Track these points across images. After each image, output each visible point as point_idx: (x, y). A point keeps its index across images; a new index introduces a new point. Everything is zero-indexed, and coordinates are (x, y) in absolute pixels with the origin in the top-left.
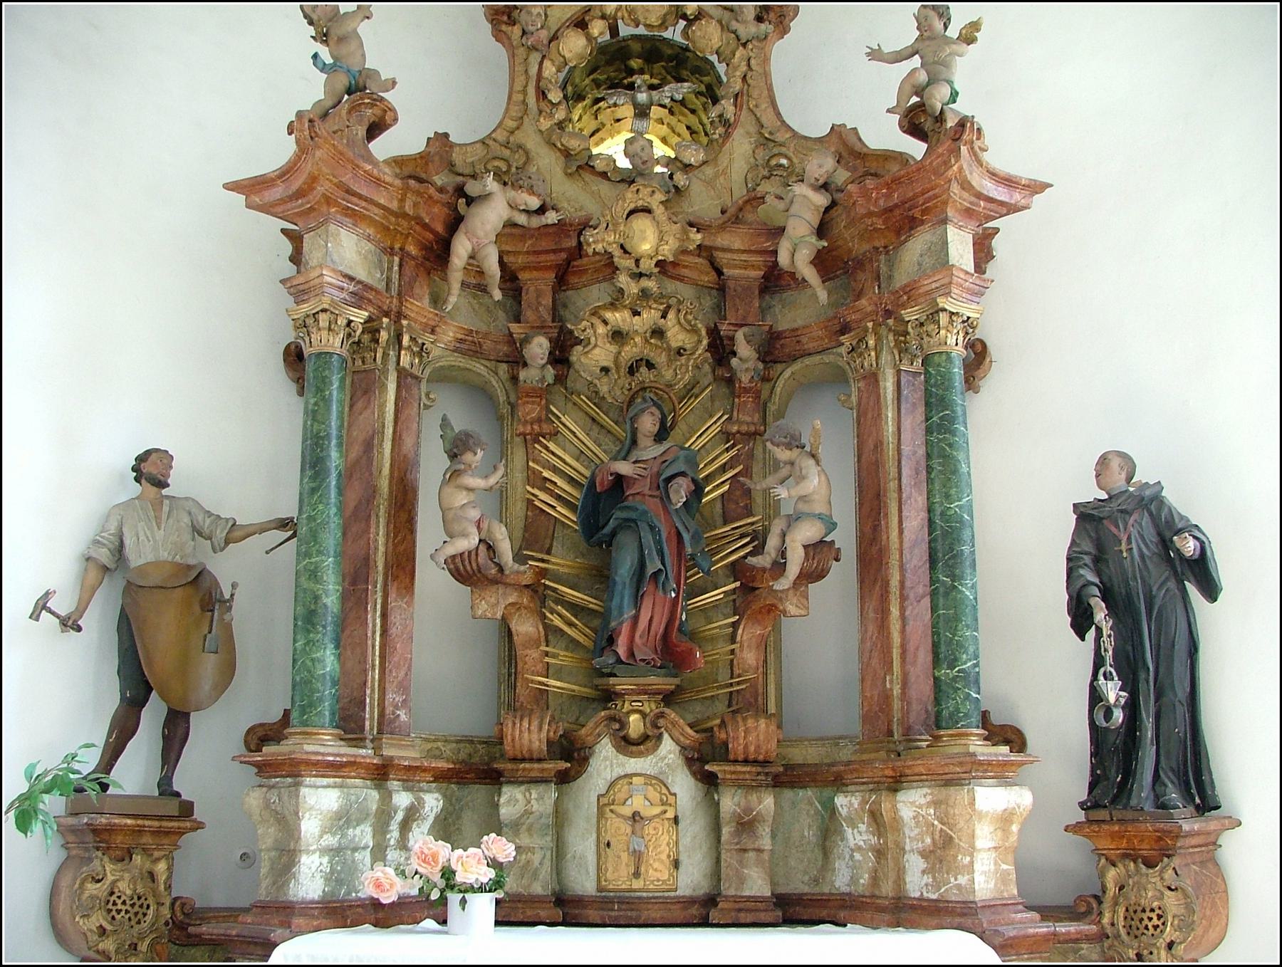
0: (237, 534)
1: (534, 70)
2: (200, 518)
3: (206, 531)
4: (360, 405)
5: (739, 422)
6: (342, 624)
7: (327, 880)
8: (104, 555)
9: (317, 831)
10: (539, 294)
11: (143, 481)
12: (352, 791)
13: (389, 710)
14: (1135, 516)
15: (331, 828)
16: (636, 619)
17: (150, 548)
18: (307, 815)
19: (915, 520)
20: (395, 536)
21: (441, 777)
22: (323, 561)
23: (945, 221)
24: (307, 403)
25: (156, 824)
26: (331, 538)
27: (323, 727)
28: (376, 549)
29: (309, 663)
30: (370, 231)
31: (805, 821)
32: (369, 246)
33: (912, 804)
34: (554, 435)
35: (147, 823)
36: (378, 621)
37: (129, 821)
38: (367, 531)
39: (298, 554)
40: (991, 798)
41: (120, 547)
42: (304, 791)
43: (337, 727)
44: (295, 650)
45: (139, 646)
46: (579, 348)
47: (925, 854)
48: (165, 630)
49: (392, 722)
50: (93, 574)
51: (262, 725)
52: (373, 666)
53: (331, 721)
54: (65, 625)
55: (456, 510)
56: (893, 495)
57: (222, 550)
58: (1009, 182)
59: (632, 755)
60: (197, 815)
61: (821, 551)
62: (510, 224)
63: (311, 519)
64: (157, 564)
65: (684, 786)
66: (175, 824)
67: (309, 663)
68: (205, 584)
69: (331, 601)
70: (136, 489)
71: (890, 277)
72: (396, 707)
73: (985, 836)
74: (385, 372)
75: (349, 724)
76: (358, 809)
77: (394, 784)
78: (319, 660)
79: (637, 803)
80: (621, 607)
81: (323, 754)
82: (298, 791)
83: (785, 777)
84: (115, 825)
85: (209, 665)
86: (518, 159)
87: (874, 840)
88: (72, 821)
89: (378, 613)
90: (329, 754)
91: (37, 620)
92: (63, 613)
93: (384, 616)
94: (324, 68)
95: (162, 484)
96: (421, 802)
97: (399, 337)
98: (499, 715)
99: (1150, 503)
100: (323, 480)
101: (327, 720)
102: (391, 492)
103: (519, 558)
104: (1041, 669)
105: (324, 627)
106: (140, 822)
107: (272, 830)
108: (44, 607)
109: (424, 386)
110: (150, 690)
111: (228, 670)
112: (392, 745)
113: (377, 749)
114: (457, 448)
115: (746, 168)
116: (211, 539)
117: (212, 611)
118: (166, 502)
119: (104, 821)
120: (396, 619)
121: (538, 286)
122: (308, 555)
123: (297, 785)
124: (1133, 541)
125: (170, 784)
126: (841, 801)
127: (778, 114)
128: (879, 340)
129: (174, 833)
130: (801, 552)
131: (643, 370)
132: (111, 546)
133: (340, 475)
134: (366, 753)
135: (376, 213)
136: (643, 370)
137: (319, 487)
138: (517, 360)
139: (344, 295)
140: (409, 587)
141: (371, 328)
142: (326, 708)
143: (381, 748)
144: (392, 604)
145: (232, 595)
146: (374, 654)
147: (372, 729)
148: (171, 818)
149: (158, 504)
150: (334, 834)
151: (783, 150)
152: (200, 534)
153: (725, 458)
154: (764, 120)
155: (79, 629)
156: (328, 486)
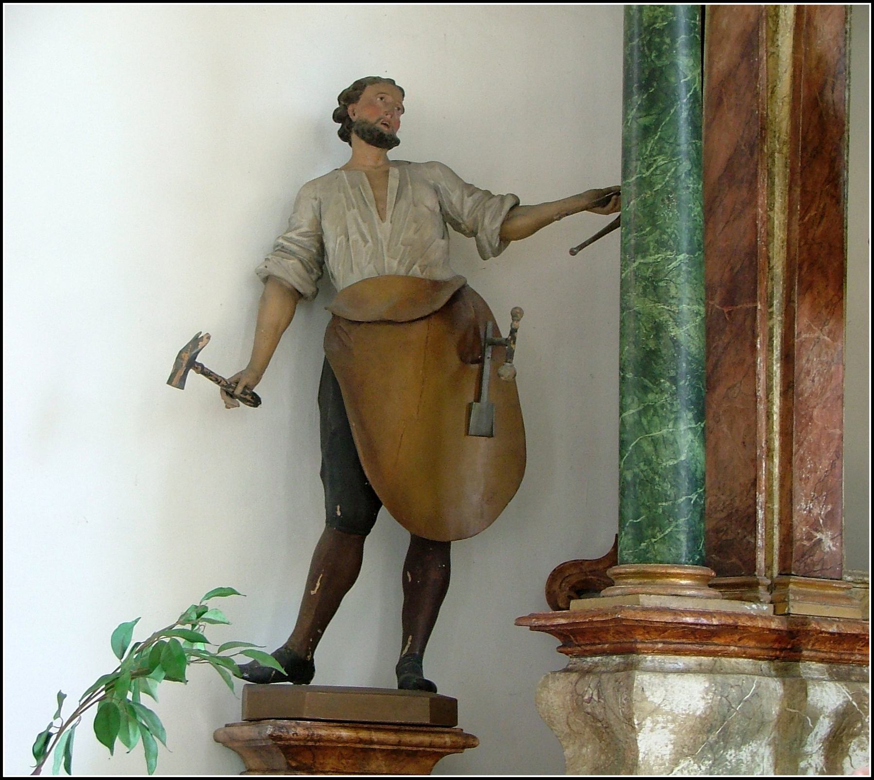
0: (520, 222)
2: (455, 198)
3: (466, 220)
6: (708, 379)
8: (292, 272)
9: (667, 752)
11: (354, 137)
12: (732, 680)
13: (801, 530)
15: (695, 747)
17: (369, 254)
18: (648, 723)
20: (805, 210)
22: (669, 261)
25: (392, 737)
26: (683, 217)
27: (676, 563)
28: (770, 234)
29: (649, 449)
35: (376, 736)
36: (777, 368)
37: (345, 733)
38: (751, 201)
39: (624, 250)
41: (318, 262)
42: (641, 678)
43: (703, 563)
44: (622, 423)
45: (353, 424)
48: (399, 393)
49: (805, 553)
50: (276, 306)
51: (577, 564)
52: (770, 450)
53: (692, 551)
54: (231, 395)
57: (497, 252)
60: (465, 722)
63: (644, 183)
64: (380, 282)
66: (425, 739)
67: (649, 449)
68: (467, 314)
69: (686, 332)
70: (343, 152)
72: (815, 526)
75: (726, 559)
76: (742, 712)
77: (811, 669)
78: (665, 440)
81: (675, 612)
82: (630, 679)
84: (320, 739)
85: (477, 458)
88: (250, 732)
89: (777, 353)
90: (692, 613)
91: (182, 387)
92: (227, 373)
93: (788, 358)
95: (384, 140)
100: (665, 111)
101: (684, 550)
102: (794, 127)
105: (674, 380)
106: (364, 735)
107: (588, 750)
108: (192, 364)
110: (378, 505)
111: (513, 465)
112: (806, 596)
113: (779, 603)
116: (473, 233)
117: (481, 361)
118: (394, 171)
119: (301, 731)
120: (810, 361)
122: (641, 250)
123: (630, 667)
125: (419, 670)
129: (426, 755)
132: (304, 255)
133: (696, 99)
134: (757, 611)
137: (657, 124)
142: (681, 529)
143: (785, 601)
145: (513, 331)
146: (769, 430)
147: (769, 567)
148: (416, 728)
149: (378, 177)
150: (699, 759)
152: (457, 226)
155: (256, 401)
156: (674, 122)
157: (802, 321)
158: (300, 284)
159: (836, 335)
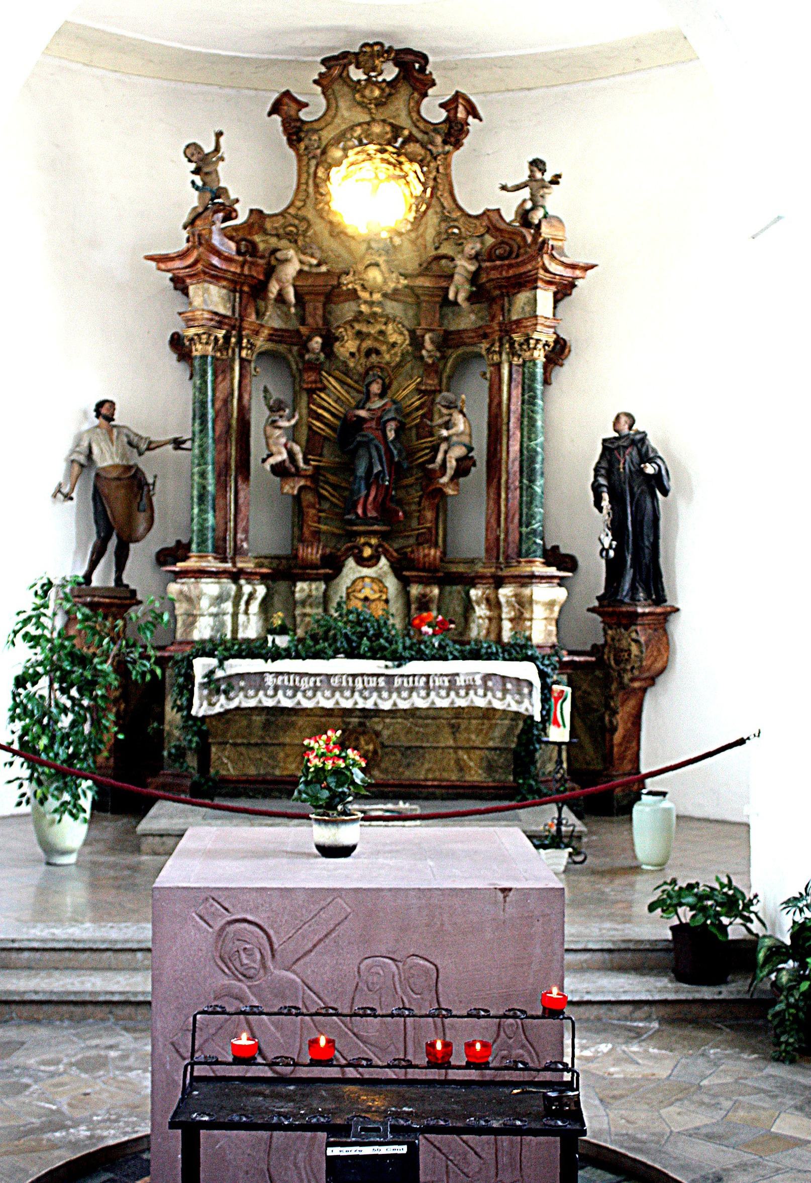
0: (153, 446)
1: (312, 170)
4: (220, 378)
5: (426, 384)
7: (212, 629)
8: (82, 459)
10: (315, 308)
14: (629, 450)
16: (367, 496)
17: (107, 457)
19: (515, 448)
21: (264, 578)
23: (536, 288)
24: (195, 384)
30: (224, 283)
31: (456, 602)
32: (224, 291)
33: (506, 592)
34: (324, 389)
38: (226, 448)
40: (542, 593)
46: (337, 344)
47: (511, 620)
50: (76, 468)
55: (273, 443)
56: (505, 433)
58: (573, 267)
59: (364, 566)
60: (139, 597)
61: (464, 466)
62: (300, 272)
65: (392, 584)
68: (139, 475)
70: (97, 422)
71: (509, 310)
72: (242, 541)
73: (539, 612)
74: (233, 360)
75: (220, 553)
77: (242, 582)
79: (367, 592)
80: (359, 489)
83: (446, 579)
86: (303, 226)
87: (488, 613)
94: (197, 188)
95: (110, 419)
96: (255, 590)
97: (239, 342)
98: (293, 545)
99: (639, 442)
103: (306, 461)
104: (582, 524)
108: (59, 491)
109: (253, 365)
114: (276, 408)
115: (434, 233)
118: (115, 431)
120: (242, 495)
121: (315, 308)
124: (626, 462)
126: (473, 592)
127: (454, 200)
128: (501, 346)
130: (454, 463)
131: (374, 356)
135: (229, 276)
136: (374, 356)
138: (304, 347)
139: (213, 323)
140: (247, 478)
141: (227, 338)
144: (240, 487)
151: (456, 224)
153: (418, 403)
154: (445, 204)
157: (240, 482)
158: (82, 463)
159: (248, 485)
